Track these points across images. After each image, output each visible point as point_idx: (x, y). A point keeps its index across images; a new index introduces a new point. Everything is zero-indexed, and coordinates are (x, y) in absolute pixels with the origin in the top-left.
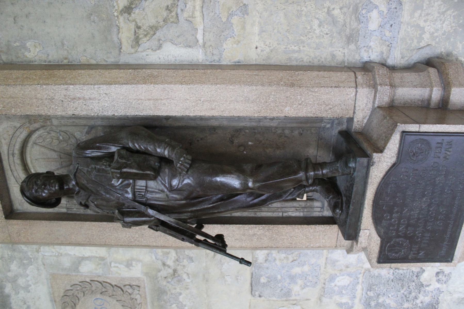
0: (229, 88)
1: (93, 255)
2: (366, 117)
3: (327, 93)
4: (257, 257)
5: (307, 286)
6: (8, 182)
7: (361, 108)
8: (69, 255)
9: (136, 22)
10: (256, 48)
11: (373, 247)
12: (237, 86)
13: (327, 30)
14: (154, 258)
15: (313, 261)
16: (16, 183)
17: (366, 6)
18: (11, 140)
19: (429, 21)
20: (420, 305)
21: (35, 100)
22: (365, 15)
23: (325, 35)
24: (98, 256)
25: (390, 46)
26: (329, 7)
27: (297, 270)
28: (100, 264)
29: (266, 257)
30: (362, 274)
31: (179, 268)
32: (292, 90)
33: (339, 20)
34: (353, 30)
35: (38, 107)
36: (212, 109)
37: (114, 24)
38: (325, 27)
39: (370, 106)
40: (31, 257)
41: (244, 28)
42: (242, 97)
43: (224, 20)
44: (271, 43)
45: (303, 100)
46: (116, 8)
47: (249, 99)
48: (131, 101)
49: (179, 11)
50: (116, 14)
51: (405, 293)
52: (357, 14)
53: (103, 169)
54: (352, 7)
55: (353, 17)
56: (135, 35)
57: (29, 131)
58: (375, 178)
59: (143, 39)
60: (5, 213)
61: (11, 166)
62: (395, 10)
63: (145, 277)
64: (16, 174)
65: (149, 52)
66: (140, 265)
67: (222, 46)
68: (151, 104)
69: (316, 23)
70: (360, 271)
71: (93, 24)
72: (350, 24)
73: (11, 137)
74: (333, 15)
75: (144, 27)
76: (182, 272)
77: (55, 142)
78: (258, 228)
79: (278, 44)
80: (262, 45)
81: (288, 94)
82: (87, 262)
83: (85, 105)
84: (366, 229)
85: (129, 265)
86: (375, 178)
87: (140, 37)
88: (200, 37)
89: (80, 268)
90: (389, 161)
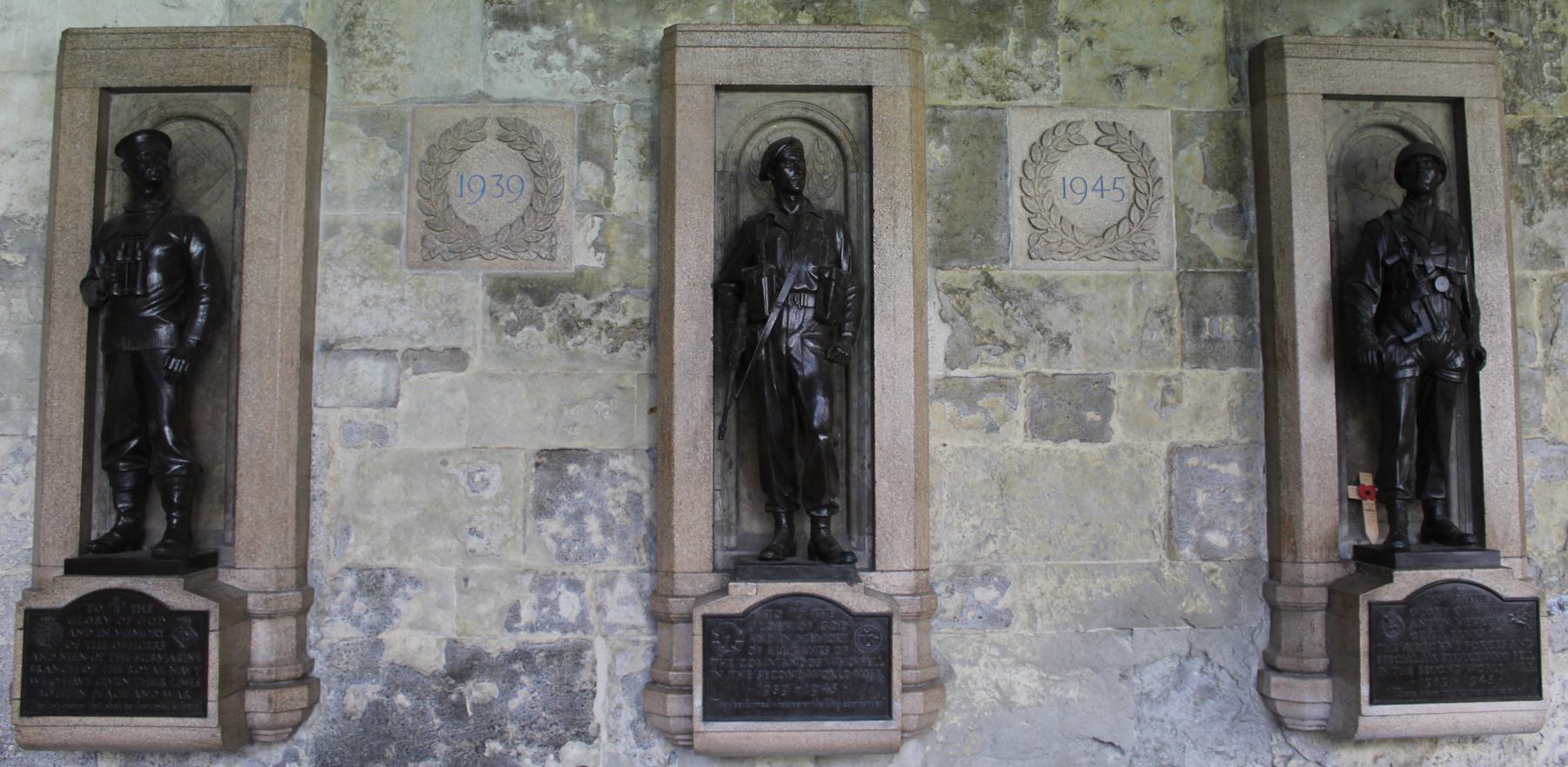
5: (560, 545)
14: (618, 289)
15: (613, 549)
20: (514, 753)
27: (592, 523)
31: (594, 329)
32: (911, 488)
39: (892, 591)
41: (970, 427)
51: (541, 721)
65: (938, 306)
66: (599, 265)
69: (977, 521)
77: (820, 168)
81: (905, 484)
82: (602, 178)
85: (597, 246)
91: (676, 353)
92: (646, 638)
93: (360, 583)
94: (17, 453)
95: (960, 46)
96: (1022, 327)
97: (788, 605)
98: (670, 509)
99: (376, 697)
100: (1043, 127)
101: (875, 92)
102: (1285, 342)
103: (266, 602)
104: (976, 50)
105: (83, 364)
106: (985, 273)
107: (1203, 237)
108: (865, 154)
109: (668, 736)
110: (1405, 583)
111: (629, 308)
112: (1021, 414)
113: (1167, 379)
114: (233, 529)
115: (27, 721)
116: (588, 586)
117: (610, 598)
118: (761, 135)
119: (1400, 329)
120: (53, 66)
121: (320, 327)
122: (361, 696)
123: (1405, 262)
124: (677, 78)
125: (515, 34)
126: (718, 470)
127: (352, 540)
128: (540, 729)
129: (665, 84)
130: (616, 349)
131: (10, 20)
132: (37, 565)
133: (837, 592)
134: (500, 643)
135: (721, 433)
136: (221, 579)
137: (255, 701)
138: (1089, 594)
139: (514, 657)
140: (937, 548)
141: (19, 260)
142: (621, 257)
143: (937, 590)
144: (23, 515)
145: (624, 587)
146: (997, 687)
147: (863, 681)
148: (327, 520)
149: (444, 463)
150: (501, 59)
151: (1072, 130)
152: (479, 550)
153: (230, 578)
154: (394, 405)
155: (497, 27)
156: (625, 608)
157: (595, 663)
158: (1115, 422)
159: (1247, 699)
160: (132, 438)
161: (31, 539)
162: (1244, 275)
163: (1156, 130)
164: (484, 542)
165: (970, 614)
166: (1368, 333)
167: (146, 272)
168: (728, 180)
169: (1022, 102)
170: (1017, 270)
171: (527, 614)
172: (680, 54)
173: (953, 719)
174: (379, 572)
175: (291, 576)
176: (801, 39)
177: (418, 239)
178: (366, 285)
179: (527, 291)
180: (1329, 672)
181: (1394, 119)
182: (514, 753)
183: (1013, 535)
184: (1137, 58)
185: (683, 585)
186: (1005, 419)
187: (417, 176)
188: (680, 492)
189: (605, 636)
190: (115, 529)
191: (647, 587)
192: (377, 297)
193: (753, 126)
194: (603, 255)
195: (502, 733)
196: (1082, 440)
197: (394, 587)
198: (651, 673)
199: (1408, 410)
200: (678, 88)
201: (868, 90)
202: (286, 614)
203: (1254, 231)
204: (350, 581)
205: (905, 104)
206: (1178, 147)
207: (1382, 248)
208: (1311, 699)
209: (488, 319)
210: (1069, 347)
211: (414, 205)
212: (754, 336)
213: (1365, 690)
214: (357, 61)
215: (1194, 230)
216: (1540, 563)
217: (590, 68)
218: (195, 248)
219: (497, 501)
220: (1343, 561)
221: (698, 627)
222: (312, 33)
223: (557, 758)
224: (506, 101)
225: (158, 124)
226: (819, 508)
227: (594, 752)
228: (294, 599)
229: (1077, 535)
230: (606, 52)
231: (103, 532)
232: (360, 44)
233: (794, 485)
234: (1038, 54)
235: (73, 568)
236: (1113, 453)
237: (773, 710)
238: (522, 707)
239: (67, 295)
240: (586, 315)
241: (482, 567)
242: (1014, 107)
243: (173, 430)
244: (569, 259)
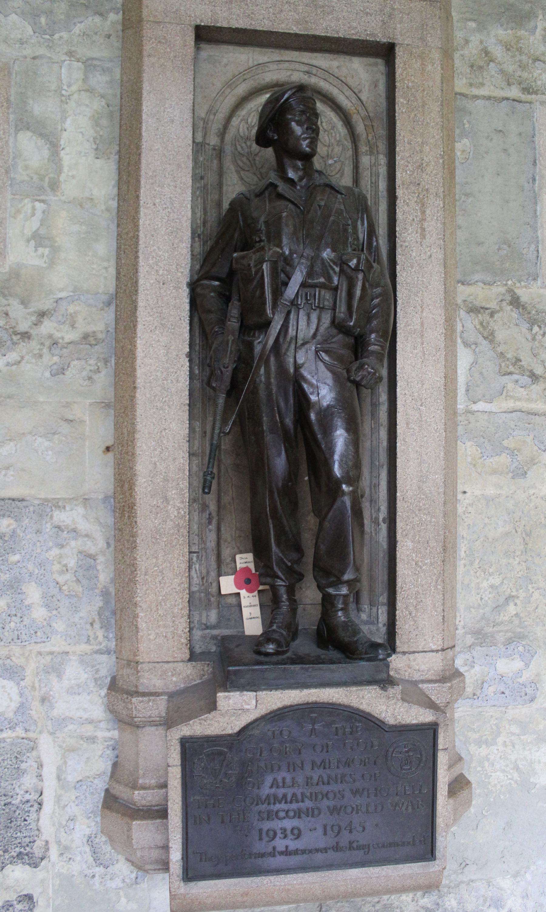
0: (440, 450)
1: (65, 169)
2: (399, 673)
3: (435, 606)
4: (68, 508)
6: (258, 49)
7: (413, 663)
8: (64, 119)
9: (498, 312)
10: (465, 492)
11: (218, 722)
12: (443, 462)
13: (487, 598)
15: (59, 626)
16: (256, 63)
17: (529, 650)
18: (337, 78)
19: (505, 749)
21: (419, 140)
22: (516, 650)
23: (480, 596)
24: (62, 178)
25: (475, 697)
26: (518, 597)
27: (33, 594)
28: (42, 179)
29: (67, 527)
30: (24, 735)
31: (34, 344)
33: (502, 614)
34: (492, 636)
35: (409, 143)
36: (407, 424)
37: (497, 278)
38: (490, 596)
39: (416, 677)
40: (56, 36)
41: (494, 472)
42: (427, 472)
43: (505, 443)
44: (469, 515)
45: (424, 568)
46: (518, 285)
47: (423, 482)
48: (419, 295)
49: (516, 377)
50: (510, 282)
52: (516, 639)
53: (348, 239)
54: (522, 630)
55: (509, 634)
56: (482, 308)
57: (351, 112)
58: (358, 697)
59: (477, 320)
60: (205, 27)
61: (287, 63)
62: (523, 694)
63: (7, 269)
64: (273, 67)
67: (469, 440)
68: (416, 327)
69: (496, 580)
70: (32, 728)
71: (497, 247)
72: (500, 632)
73: (343, 79)
74: (508, 605)
75: (492, 324)
76: (25, 351)
78: (182, 506)
79: (469, 525)
80: (467, 501)
81: (432, 544)
82: (46, 153)
83: (414, 220)
84: (257, 701)
85: (38, 239)
86: (358, 697)
87: (480, 315)
88: (481, 406)
89: (29, 134)
90: (389, 714)
95: (482, 27)
98: (133, 581)
101: (399, 52)
104: (501, 32)
106: (510, 291)
108: (382, 132)
111: (80, 319)
116: (31, 668)
117: (57, 687)
124: (145, 12)
130: (62, 371)
133: (367, 699)
145: (75, 672)
157: (40, 766)
165: (491, 689)
168: (208, 157)
183: (536, 595)
188: (146, 558)
191: (104, 672)
194: (46, 251)
200: (146, 26)
201: (386, 52)
212: (250, 346)
233: (299, 549)
240: (23, 327)
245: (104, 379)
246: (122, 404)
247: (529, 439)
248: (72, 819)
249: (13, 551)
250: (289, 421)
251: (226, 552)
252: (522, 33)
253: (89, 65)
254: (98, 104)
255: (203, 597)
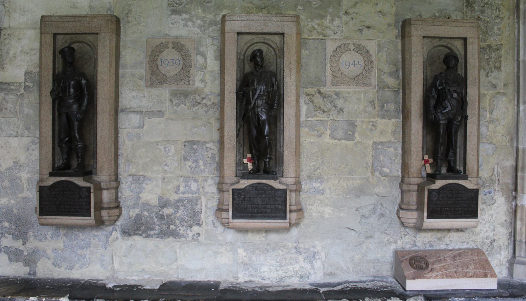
8: (207, 52)
15: (207, 170)
20: (178, 229)
27: (201, 163)
31: (201, 105)
41: (313, 136)
66: (203, 86)
69: (315, 164)
77: (269, 58)
82: (203, 60)
85: (202, 81)
88: (309, 119)
91: (225, 113)
92: (217, 196)
93: (133, 180)
94: (33, 142)
96: (329, 106)
97: (257, 186)
98: (223, 159)
99: (139, 213)
100: (337, 45)
102: (408, 112)
103: (106, 185)
105: (52, 116)
106: (318, 90)
107: (385, 80)
109: (223, 224)
110: (439, 184)
112: (328, 132)
113: (372, 122)
114: (96, 164)
115: (41, 217)
116: (200, 181)
117: (206, 184)
118: (251, 47)
119: (442, 108)
120: (39, 26)
121: (120, 104)
122: (134, 213)
123: (444, 89)
125: (177, 16)
126: (238, 147)
127: (131, 167)
128: (186, 222)
129: (223, 32)
130: (208, 111)
131: (24, 12)
132: (41, 174)
133: (271, 183)
134: (174, 197)
135: (237, 136)
136: (93, 178)
137: (104, 213)
138: (347, 185)
139: (178, 201)
140: (302, 171)
141: (31, 85)
142: (209, 84)
143: (302, 183)
144: (36, 160)
145: (210, 181)
146: (319, 212)
147: (278, 208)
148: (123, 161)
149: (157, 145)
150: (173, 24)
151: (346, 46)
152: (168, 170)
153: (95, 178)
154: (143, 128)
155: (172, 14)
156: (211, 188)
158: (356, 135)
159: (393, 218)
160: (66, 138)
161: (38, 167)
162: (397, 91)
163: (372, 47)
164: (169, 168)
166: (432, 109)
167: (69, 89)
168: (240, 62)
169: (331, 37)
170: (328, 89)
171: (182, 189)
172: (227, 23)
173: (306, 221)
174: (139, 177)
175: (113, 178)
176: (263, 18)
177: (149, 79)
178: (133, 92)
179: (181, 94)
180: (417, 210)
181: (445, 44)
182: (178, 229)
183: (325, 168)
184: (367, 24)
185: (227, 181)
186: (323, 133)
187: (148, 59)
188: (226, 154)
189: (205, 196)
190: (63, 164)
191: (217, 181)
192: (137, 96)
193: (248, 45)
195: (175, 223)
196: (346, 140)
197: (143, 181)
198: (218, 206)
199: (443, 133)
201: (283, 34)
202: (112, 188)
203: (401, 78)
204: (130, 179)
205: (294, 38)
206: (379, 51)
207: (438, 84)
208: (411, 217)
209: (170, 102)
210: (343, 112)
211: (147, 67)
212: (248, 108)
213: (425, 215)
214: (129, 24)
215: (383, 77)
216: (484, 180)
217: (200, 27)
218: (83, 82)
219: (173, 156)
220: (422, 177)
221: (231, 192)
222: (116, 17)
223: (191, 230)
224: (174, 37)
225: (70, 44)
226: (266, 158)
227: (201, 229)
228: (114, 184)
229: (344, 168)
230: (204, 22)
231: (59, 165)
232: (130, 19)
234: (336, 23)
235: (52, 174)
236: (356, 144)
237: (252, 216)
238: (180, 216)
239: (46, 95)
240: (199, 101)
241: (169, 175)
242: (328, 39)
243: (78, 135)
244: (194, 84)
245: (217, 113)
246: (221, 119)
247: (322, 127)
248: (209, 216)
249: (196, 153)
250: (256, 124)
251: (245, 154)
252: (323, 21)
253: (213, 38)
254: (215, 48)
255: (239, 164)
